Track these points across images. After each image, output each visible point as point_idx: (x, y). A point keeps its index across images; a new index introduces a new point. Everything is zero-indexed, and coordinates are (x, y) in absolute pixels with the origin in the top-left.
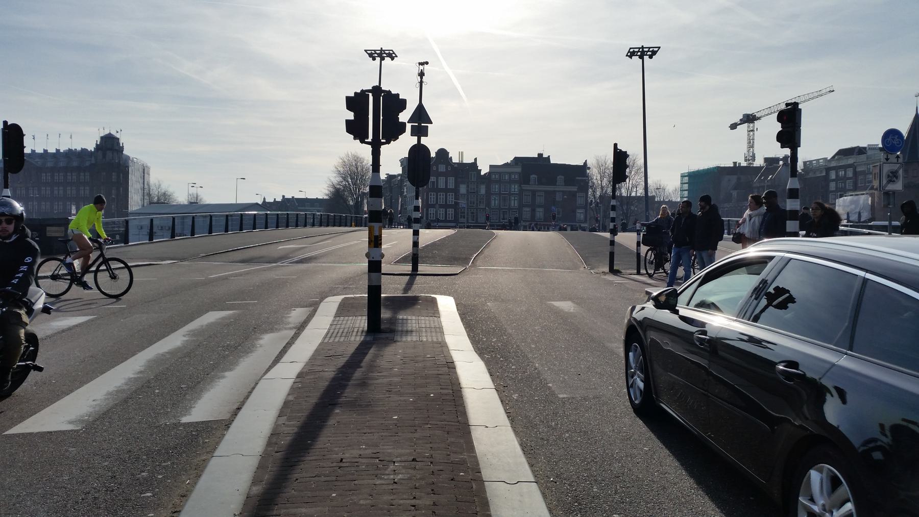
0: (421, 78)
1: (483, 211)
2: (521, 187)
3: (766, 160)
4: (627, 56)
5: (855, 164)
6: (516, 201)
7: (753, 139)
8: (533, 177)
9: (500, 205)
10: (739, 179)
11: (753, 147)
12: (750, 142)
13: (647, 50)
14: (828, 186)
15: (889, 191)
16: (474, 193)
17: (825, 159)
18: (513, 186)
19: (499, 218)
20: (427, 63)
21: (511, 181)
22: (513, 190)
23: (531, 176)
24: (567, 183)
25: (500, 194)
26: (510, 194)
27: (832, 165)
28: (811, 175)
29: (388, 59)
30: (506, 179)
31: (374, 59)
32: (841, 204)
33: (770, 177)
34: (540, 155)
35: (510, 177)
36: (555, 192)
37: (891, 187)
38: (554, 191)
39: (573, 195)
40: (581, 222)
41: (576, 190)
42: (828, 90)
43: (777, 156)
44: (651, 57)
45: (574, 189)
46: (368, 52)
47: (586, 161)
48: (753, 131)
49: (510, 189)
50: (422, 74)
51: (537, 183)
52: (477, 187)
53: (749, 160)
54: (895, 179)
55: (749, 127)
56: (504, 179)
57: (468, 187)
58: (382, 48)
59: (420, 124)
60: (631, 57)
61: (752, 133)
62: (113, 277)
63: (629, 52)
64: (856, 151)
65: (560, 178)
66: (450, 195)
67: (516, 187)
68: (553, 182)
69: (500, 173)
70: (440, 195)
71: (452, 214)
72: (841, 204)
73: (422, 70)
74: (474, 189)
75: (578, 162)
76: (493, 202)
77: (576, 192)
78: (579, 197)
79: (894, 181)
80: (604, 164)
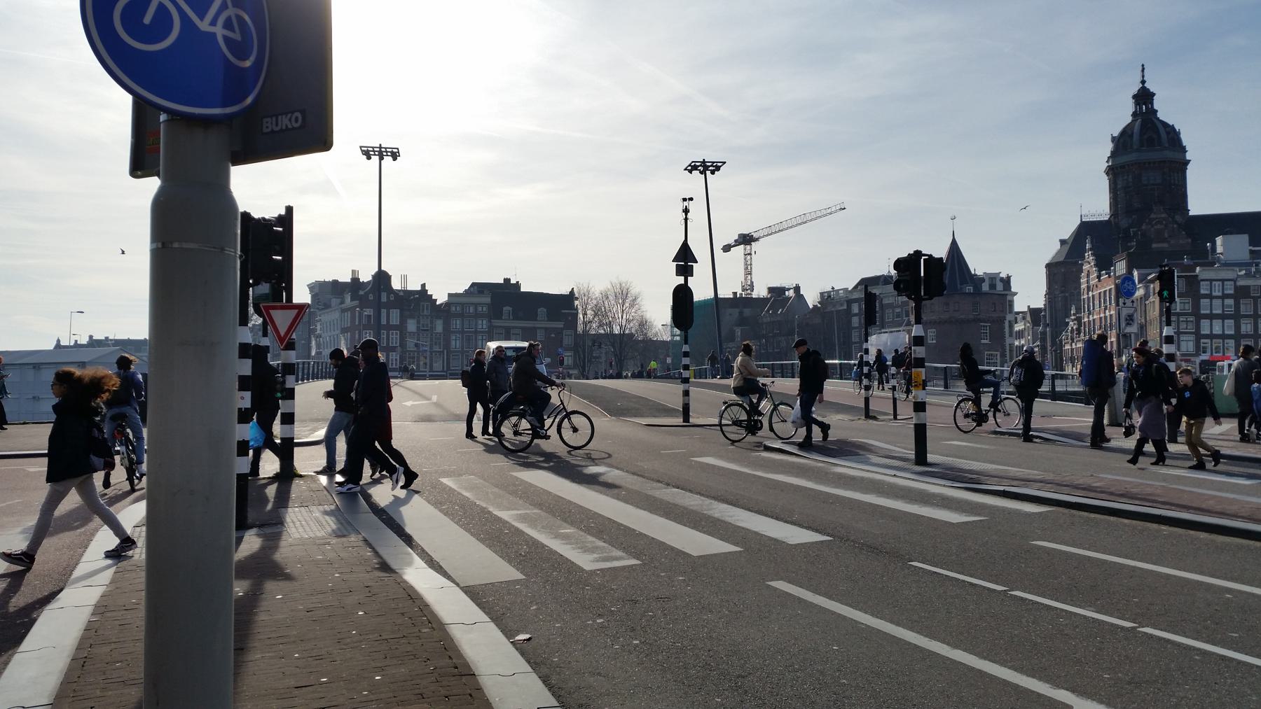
0: (686, 215)
1: (440, 355)
2: (491, 322)
3: (771, 290)
4: (686, 169)
5: (881, 296)
6: (458, 341)
7: (751, 265)
8: (507, 309)
9: (463, 346)
10: (741, 313)
11: (751, 274)
12: (747, 268)
13: (709, 164)
14: (850, 322)
15: (1127, 333)
16: (427, 330)
17: (845, 290)
18: (480, 322)
19: (462, 363)
20: (691, 199)
21: (477, 316)
22: (480, 327)
23: (505, 308)
24: (552, 316)
25: (462, 332)
26: (476, 332)
27: (854, 297)
28: (830, 309)
29: (388, 160)
30: (471, 311)
31: (369, 158)
32: (874, 343)
33: (780, 310)
34: (507, 281)
35: (476, 310)
36: (535, 329)
37: (1129, 330)
38: (534, 327)
39: (559, 332)
40: (570, 369)
41: (562, 326)
42: (838, 207)
43: (783, 285)
44: (713, 172)
45: (560, 325)
46: (363, 149)
47: (573, 289)
48: (750, 254)
49: (476, 325)
50: (686, 211)
51: (511, 317)
52: (432, 323)
53: (747, 290)
54: (1131, 322)
55: (745, 249)
56: (468, 311)
57: (418, 322)
58: (380, 145)
59: (686, 263)
60: (690, 172)
61: (749, 257)
62: (575, 430)
63: (690, 165)
64: (882, 280)
65: (542, 311)
66: (393, 333)
67: (484, 322)
68: (534, 317)
69: (462, 304)
70: (392, 334)
71: (396, 360)
72: (874, 343)
73: (686, 206)
74: (427, 325)
75: (563, 290)
76: (453, 343)
77: (562, 329)
78: (513, 334)
79: (1131, 324)
80: (587, 294)
